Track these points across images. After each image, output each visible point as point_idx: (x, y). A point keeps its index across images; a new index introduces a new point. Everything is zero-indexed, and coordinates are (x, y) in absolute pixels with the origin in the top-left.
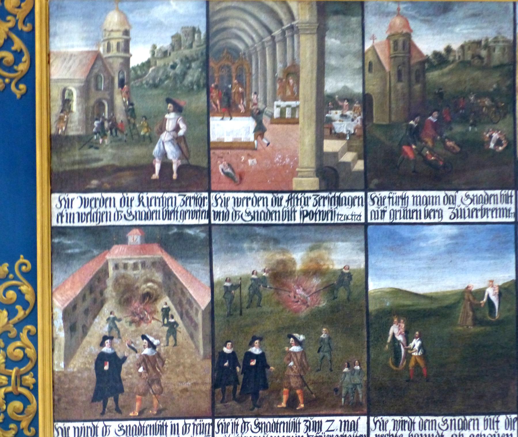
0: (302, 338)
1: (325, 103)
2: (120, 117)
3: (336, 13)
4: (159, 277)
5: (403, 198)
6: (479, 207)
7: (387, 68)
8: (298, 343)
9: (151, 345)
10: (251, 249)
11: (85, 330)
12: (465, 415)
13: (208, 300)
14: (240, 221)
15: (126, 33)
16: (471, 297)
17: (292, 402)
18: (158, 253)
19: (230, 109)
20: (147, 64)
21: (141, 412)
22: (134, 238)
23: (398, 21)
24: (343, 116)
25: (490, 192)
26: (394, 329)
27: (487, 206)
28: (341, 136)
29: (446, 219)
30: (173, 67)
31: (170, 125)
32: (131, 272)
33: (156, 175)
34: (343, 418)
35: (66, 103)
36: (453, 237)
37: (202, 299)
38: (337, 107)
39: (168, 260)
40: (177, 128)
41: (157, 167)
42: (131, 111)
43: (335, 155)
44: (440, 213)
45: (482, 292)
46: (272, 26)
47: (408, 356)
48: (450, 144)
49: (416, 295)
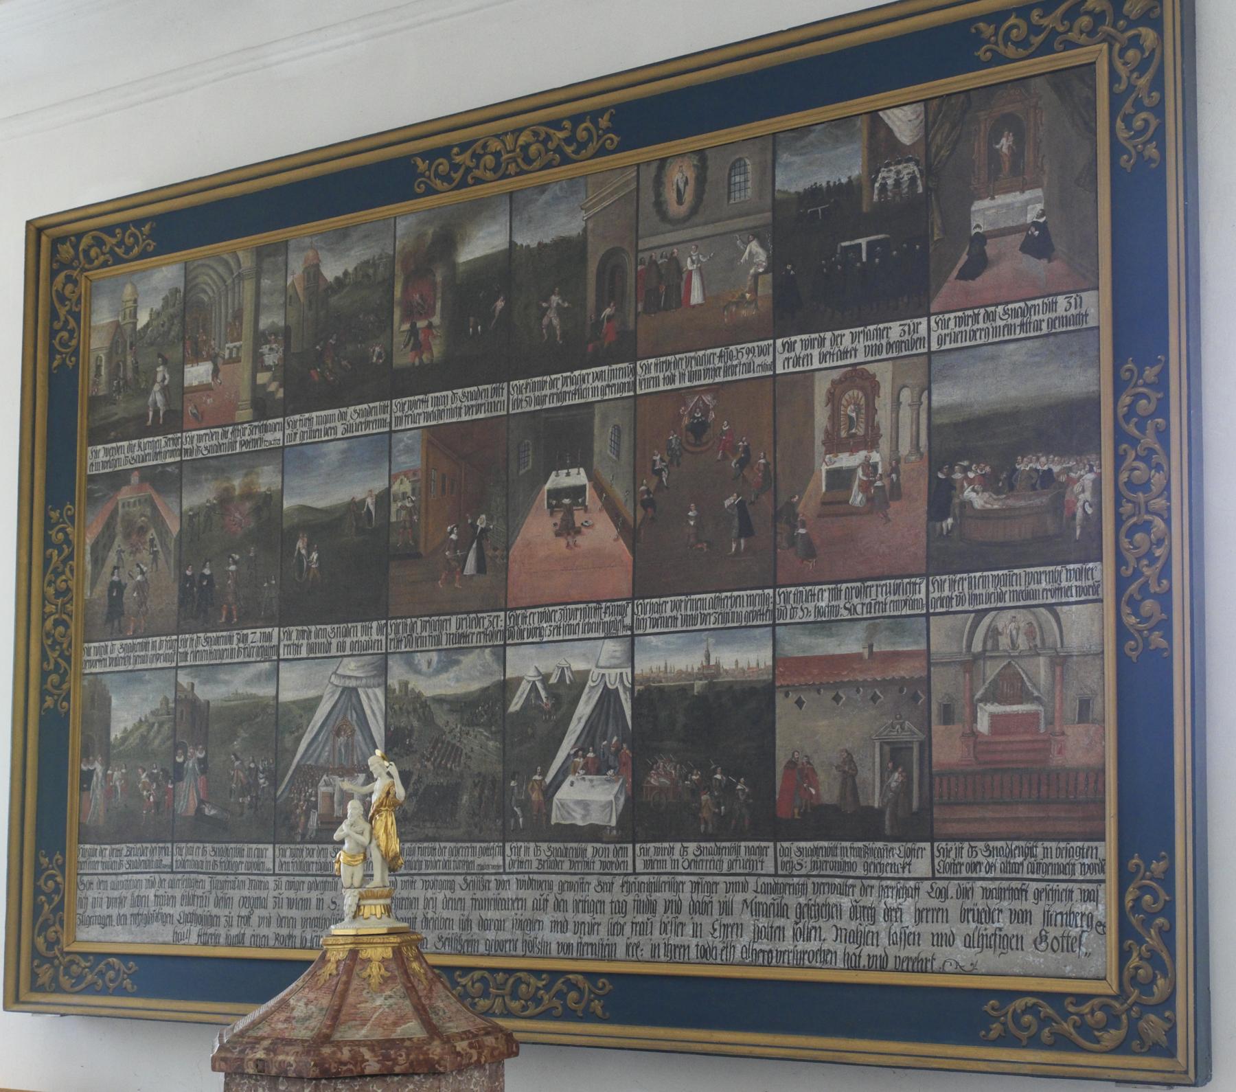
0: (237, 557)
1: (260, 338)
2: (130, 374)
3: (269, 255)
4: (148, 511)
5: (309, 419)
6: (363, 420)
7: (302, 299)
8: (235, 563)
9: (142, 573)
10: (206, 480)
11: (104, 560)
12: (347, 622)
13: (178, 529)
14: (200, 456)
15: (135, 301)
16: (355, 506)
17: (229, 619)
18: (149, 491)
19: (197, 358)
20: (147, 326)
21: (134, 632)
22: (135, 479)
23: (310, 253)
24: (271, 349)
25: (371, 405)
26: (300, 544)
27: (370, 418)
28: (268, 368)
29: (339, 436)
30: (163, 325)
31: (159, 378)
32: (132, 509)
33: (149, 423)
34: (263, 630)
35: (98, 367)
36: (344, 452)
37: (174, 527)
38: (268, 342)
39: (155, 496)
40: (164, 379)
41: (151, 414)
42: (136, 369)
43: (264, 386)
44: (335, 428)
45: (364, 501)
46: (226, 276)
47: (309, 568)
48: (344, 363)
49: (316, 509)
